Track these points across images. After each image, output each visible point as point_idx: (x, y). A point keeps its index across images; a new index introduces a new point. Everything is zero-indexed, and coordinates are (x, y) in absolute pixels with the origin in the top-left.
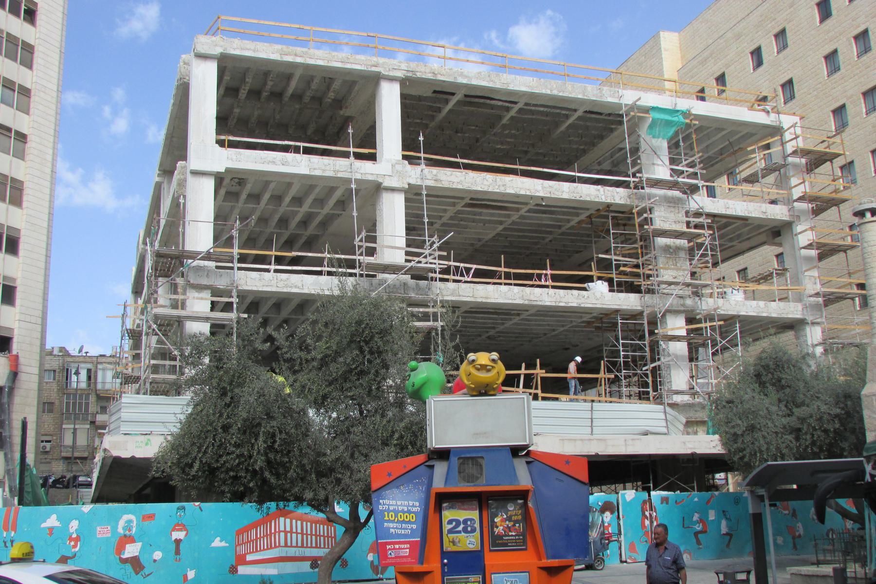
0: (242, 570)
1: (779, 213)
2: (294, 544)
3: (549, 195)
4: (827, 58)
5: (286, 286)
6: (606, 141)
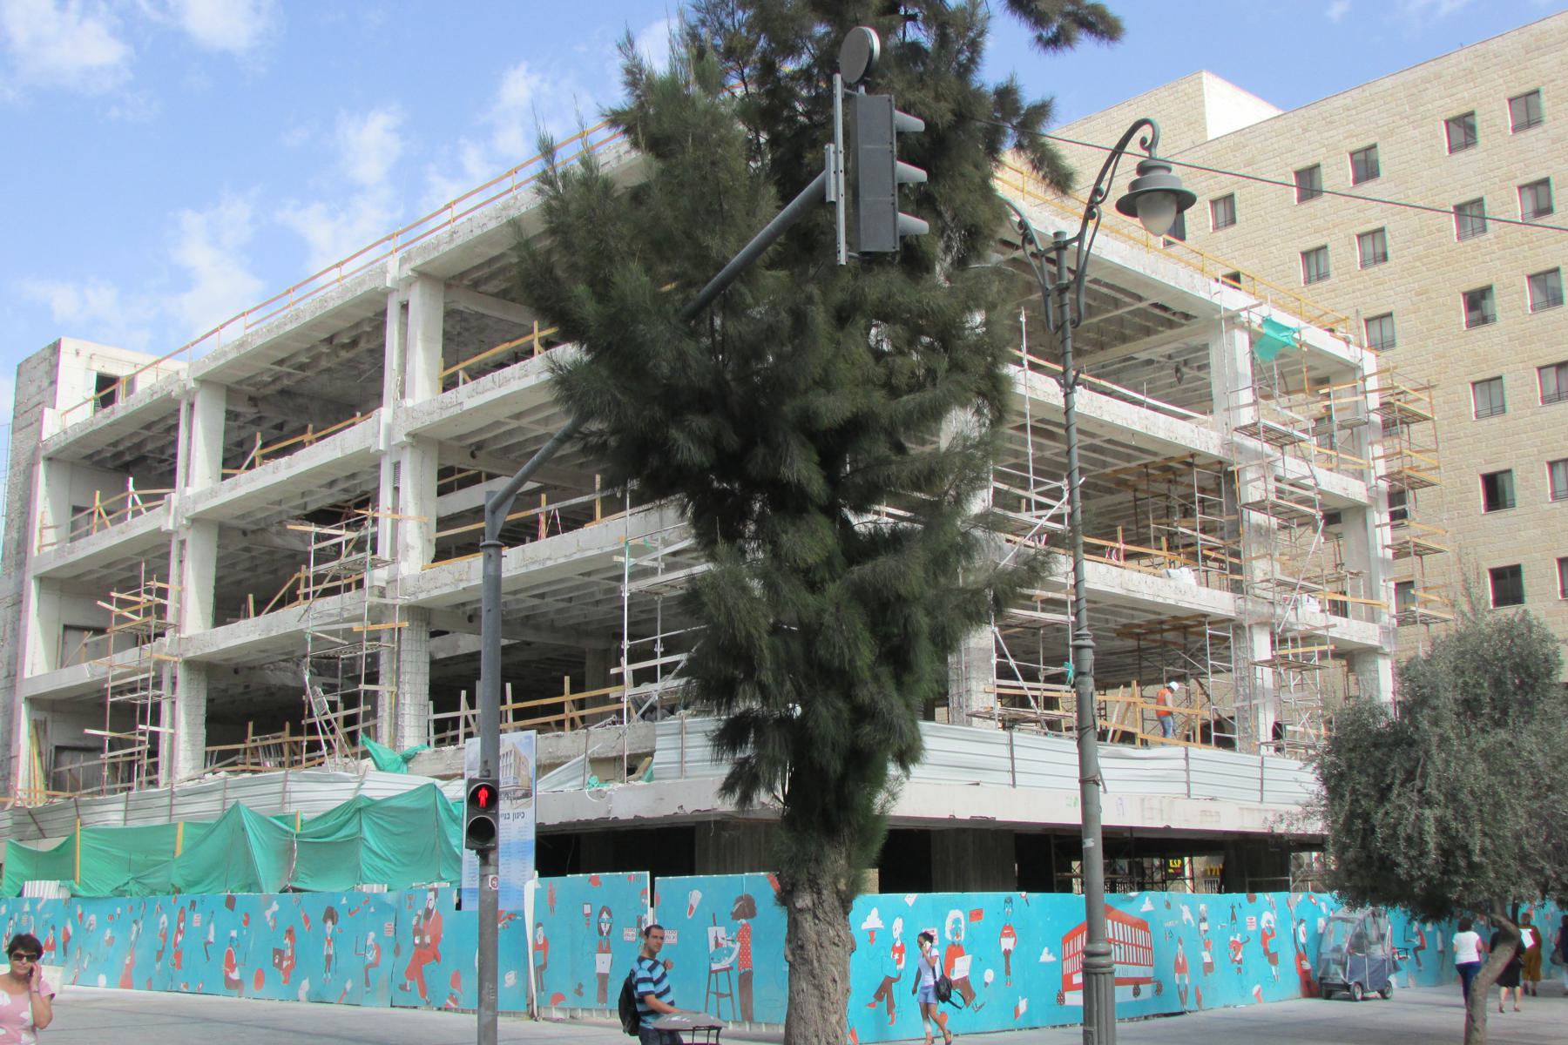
1: (1356, 491)
4: (1306, 255)
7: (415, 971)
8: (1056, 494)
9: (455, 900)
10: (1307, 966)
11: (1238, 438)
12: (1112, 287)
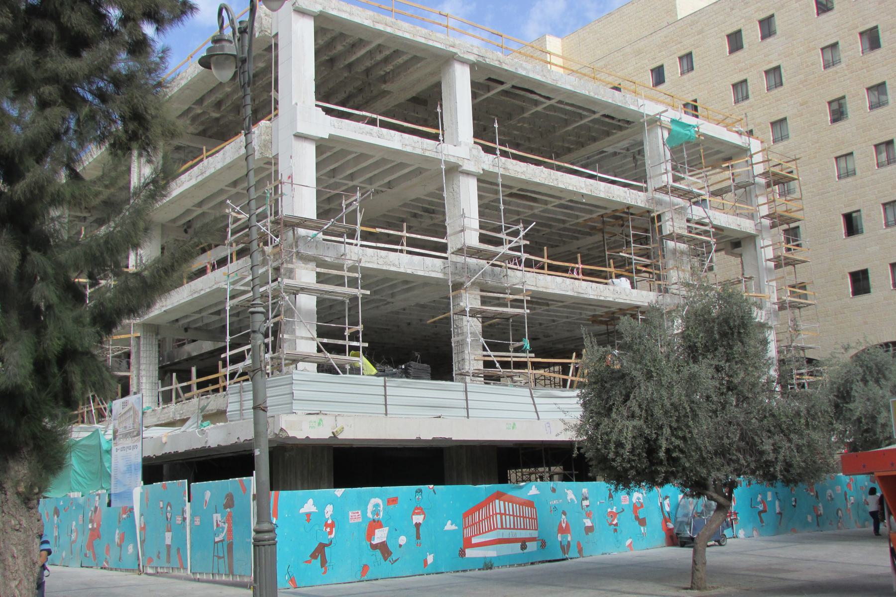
0: (469, 553)
1: (747, 226)
5: (386, 263)
6: (597, 143)
7: (90, 546)
8: (515, 234)
9: (107, 501)
10: (671, 526)
11: (659, 196)
12: (572, 105)
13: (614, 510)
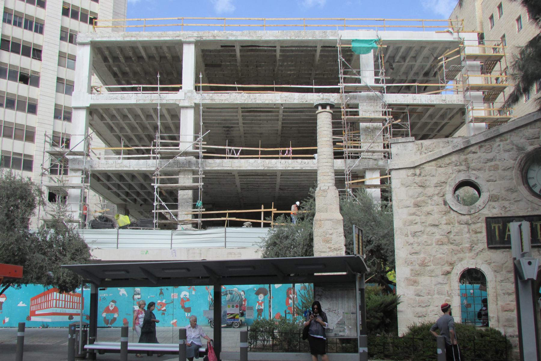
0: (33, 319)
2: (60, 306)
3: (284, 102)
5: (121, 167)
13: (164, 301)
